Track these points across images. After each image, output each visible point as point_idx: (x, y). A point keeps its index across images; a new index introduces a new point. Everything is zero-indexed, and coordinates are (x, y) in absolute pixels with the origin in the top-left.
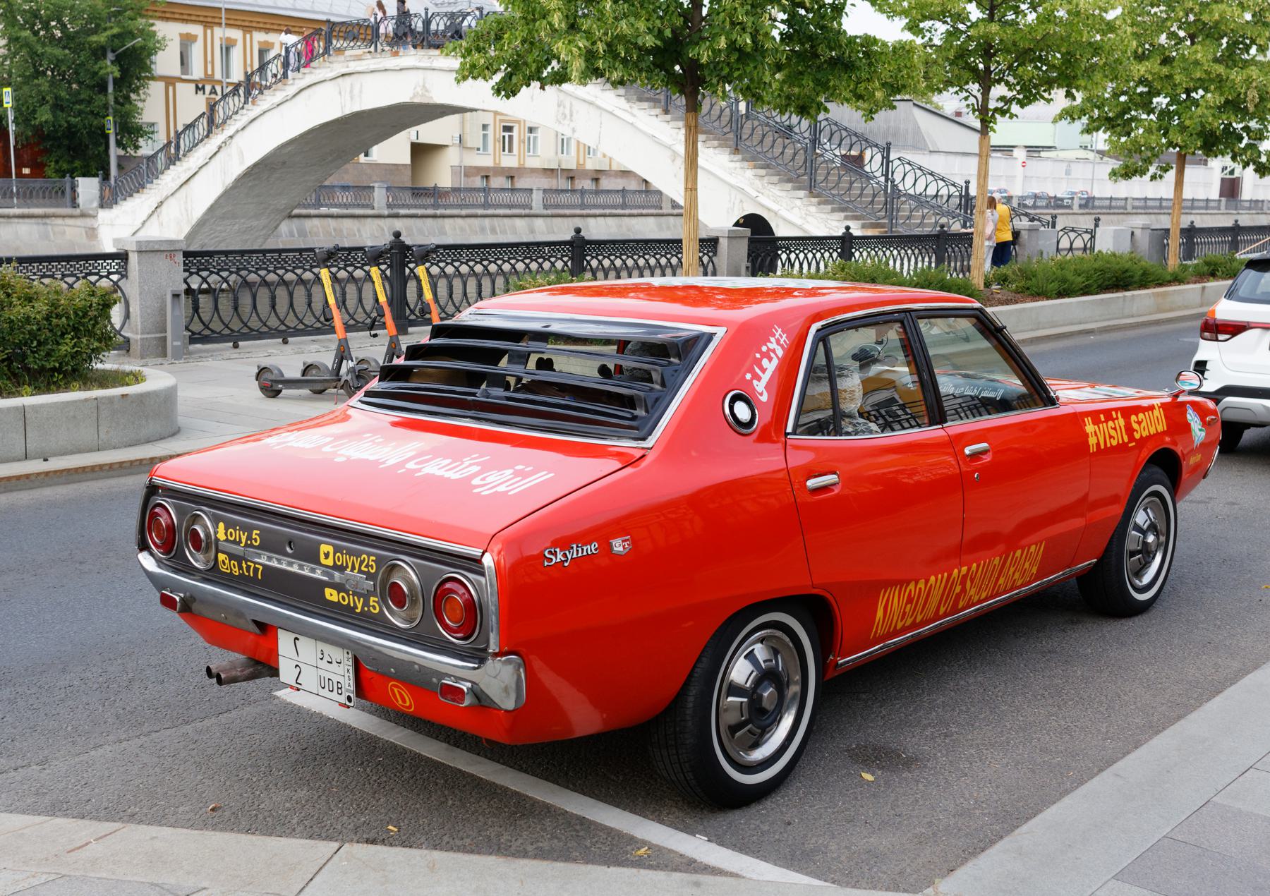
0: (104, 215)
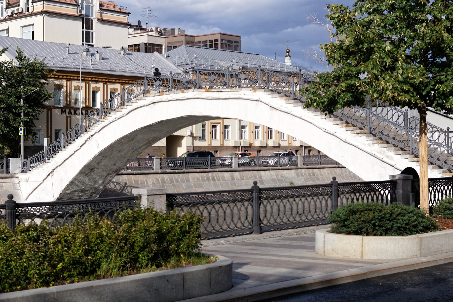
0: (23, 176)
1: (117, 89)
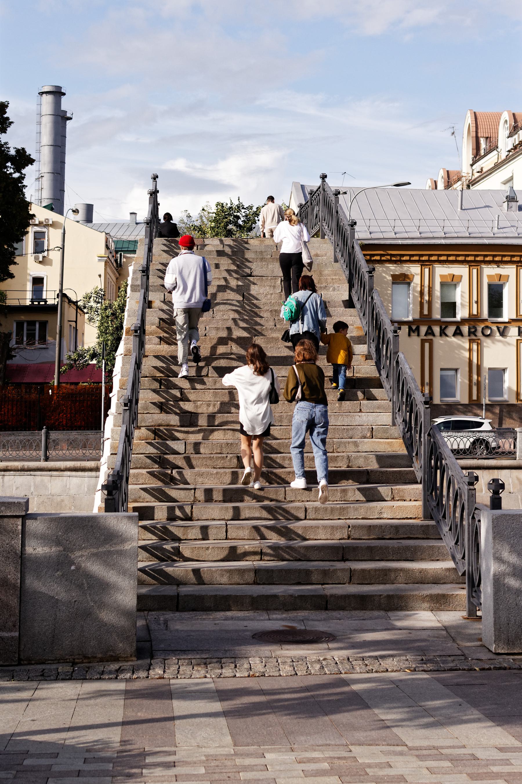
1: (461, 277)
